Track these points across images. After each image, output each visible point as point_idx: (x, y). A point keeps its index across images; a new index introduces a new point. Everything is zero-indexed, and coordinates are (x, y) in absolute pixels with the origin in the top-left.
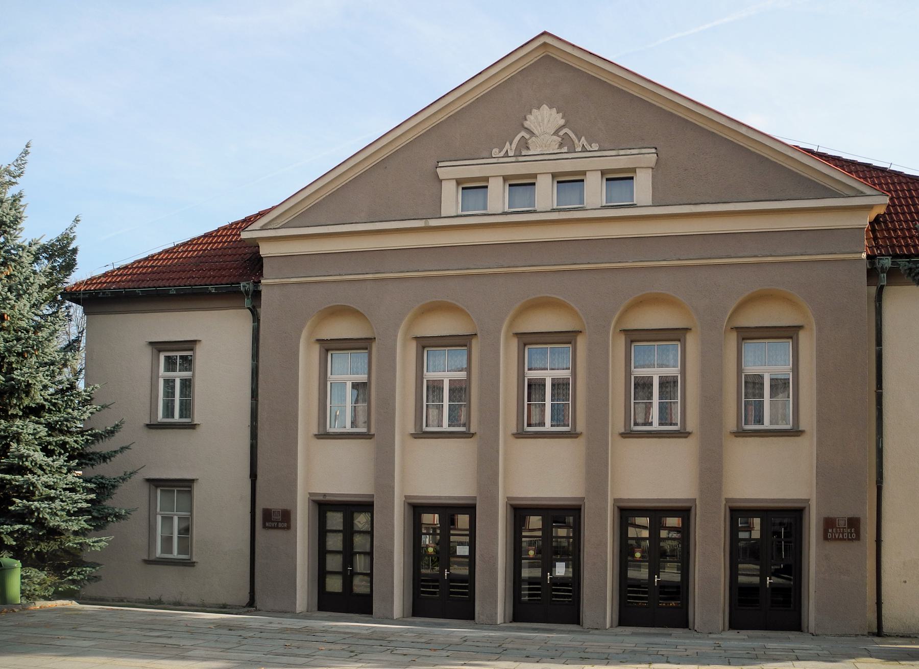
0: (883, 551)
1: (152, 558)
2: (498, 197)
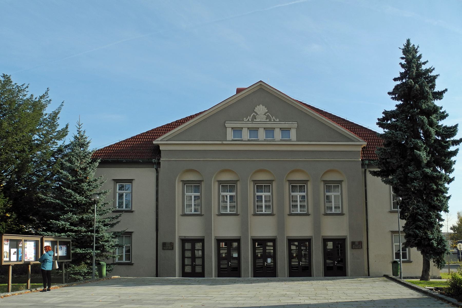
0: (155, 265)
1: (115, 262)
2: (246, 135)
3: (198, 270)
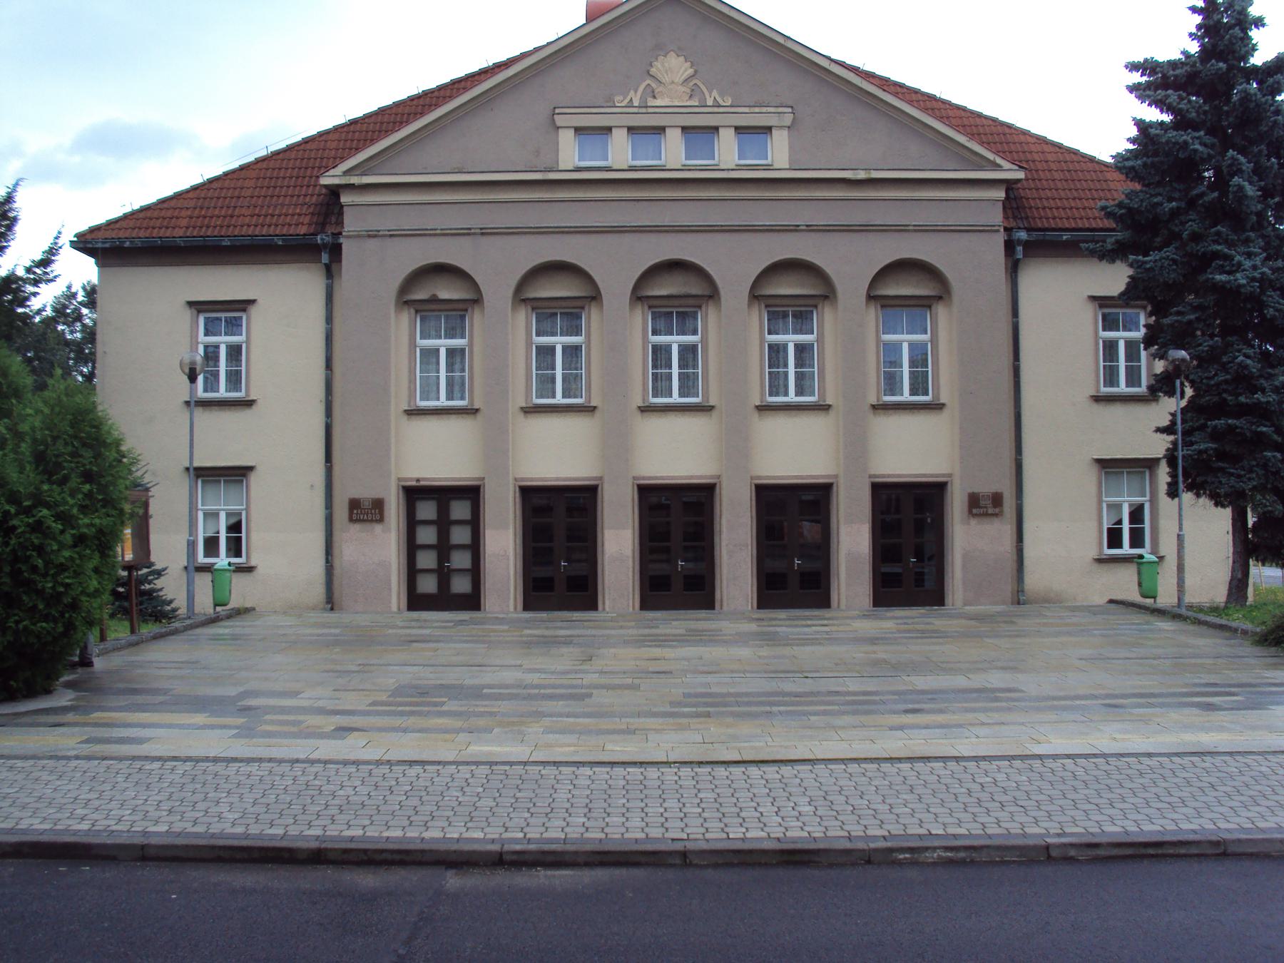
3: (461, 585)
